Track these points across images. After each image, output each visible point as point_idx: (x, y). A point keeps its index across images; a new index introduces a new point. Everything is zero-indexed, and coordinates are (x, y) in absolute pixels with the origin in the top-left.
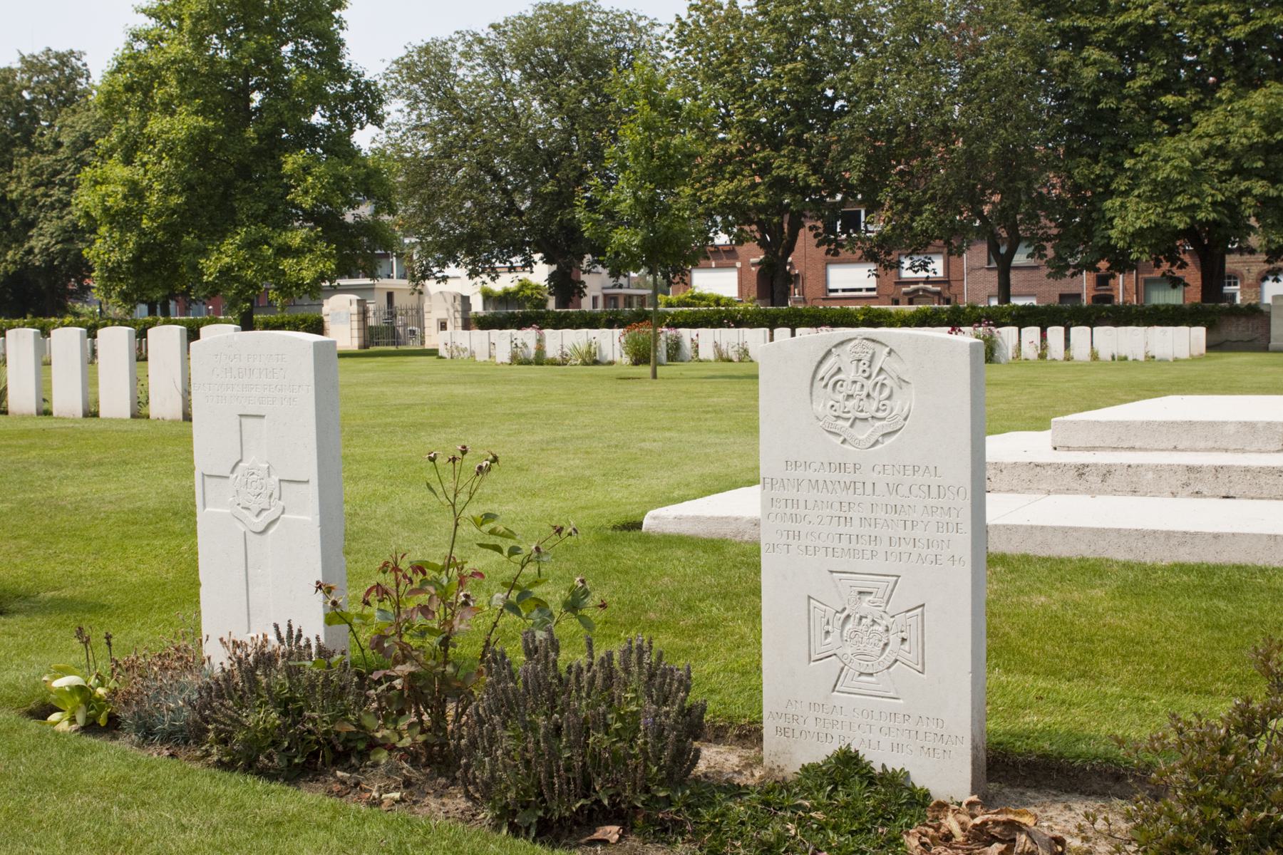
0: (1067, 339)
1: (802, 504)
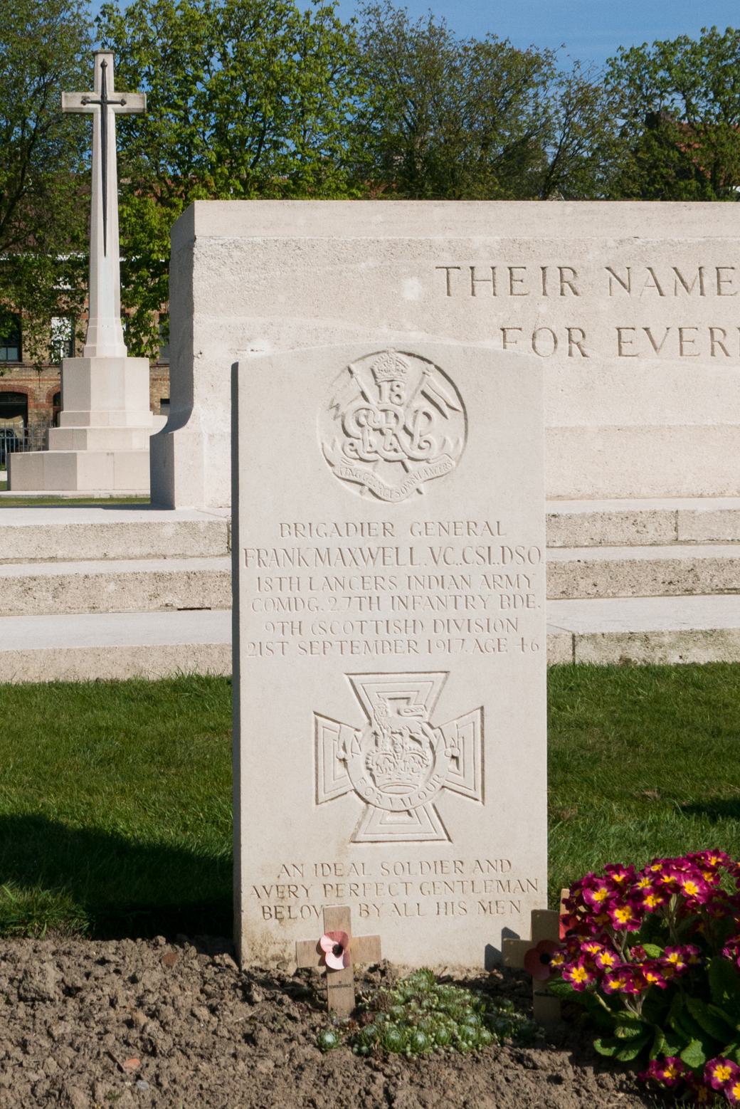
1: (305, 583)
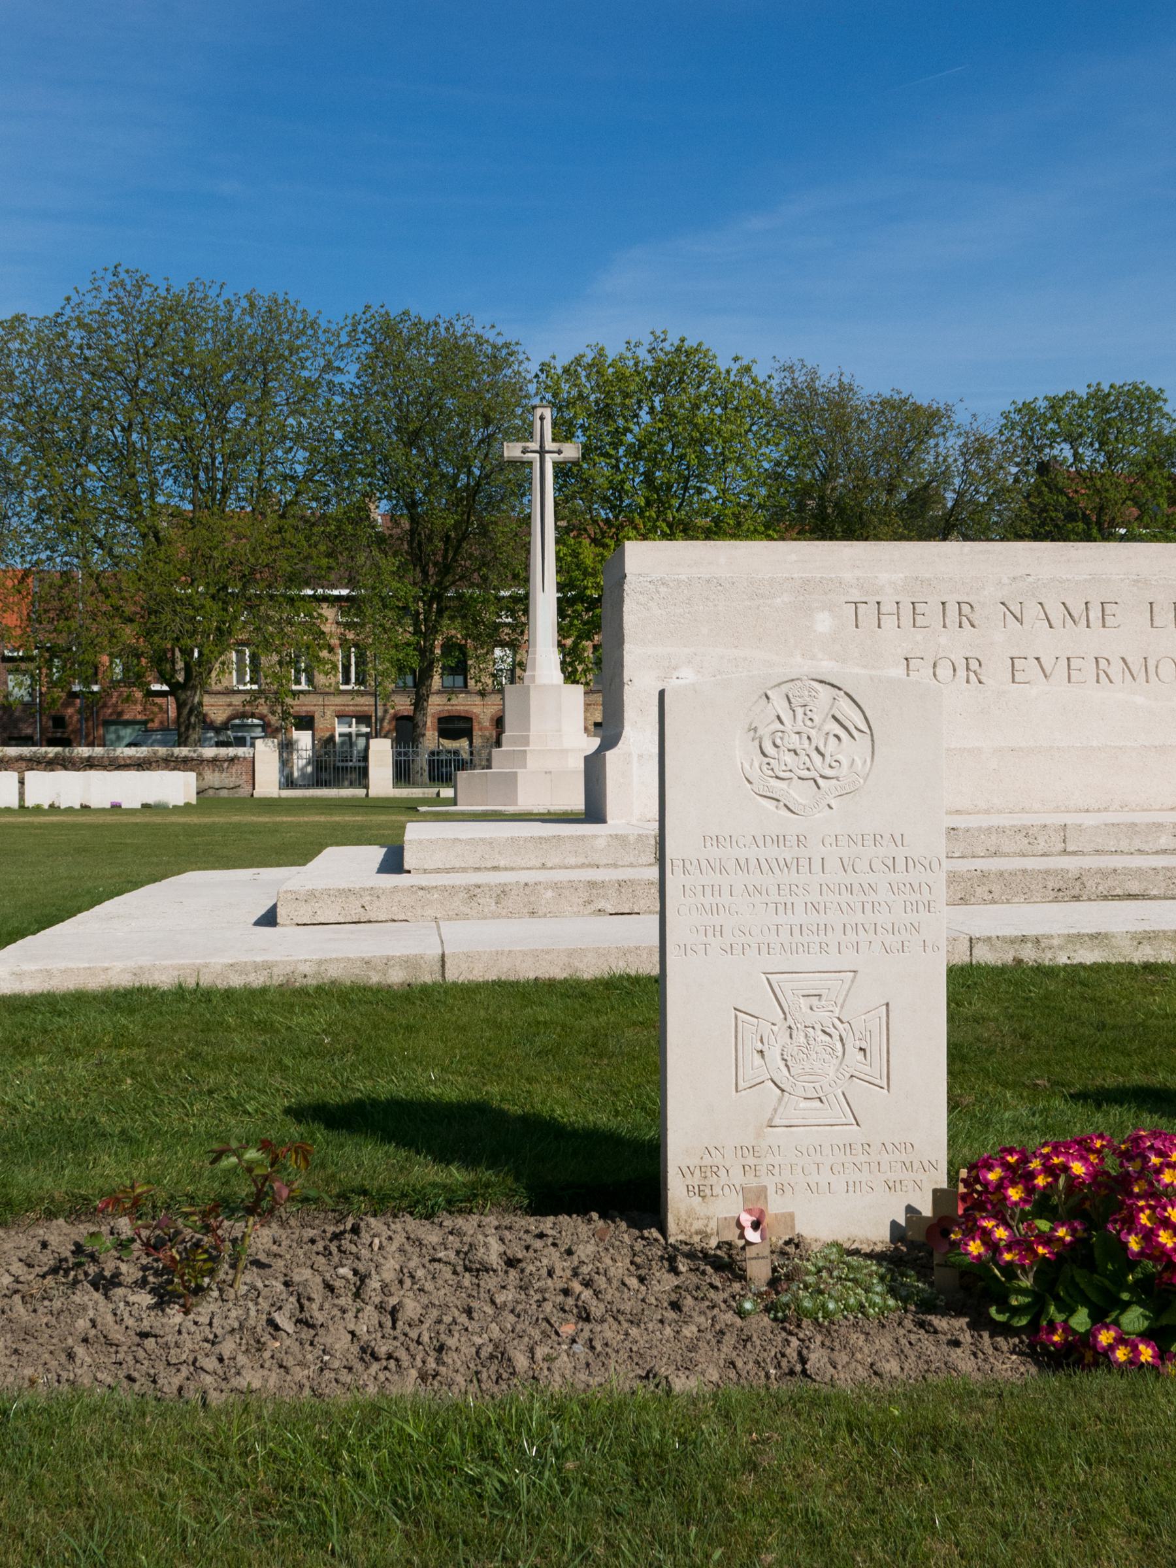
0: (22, 782)
1: (726, 890)
